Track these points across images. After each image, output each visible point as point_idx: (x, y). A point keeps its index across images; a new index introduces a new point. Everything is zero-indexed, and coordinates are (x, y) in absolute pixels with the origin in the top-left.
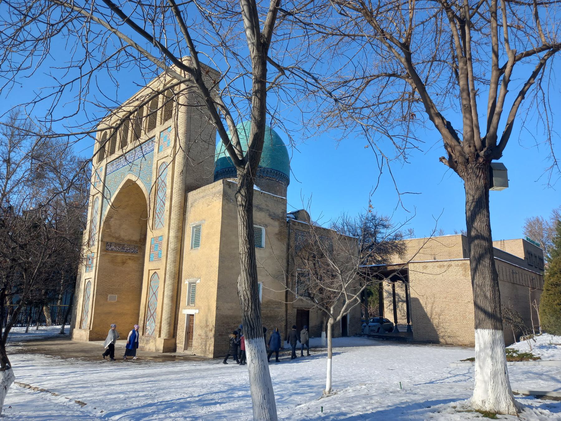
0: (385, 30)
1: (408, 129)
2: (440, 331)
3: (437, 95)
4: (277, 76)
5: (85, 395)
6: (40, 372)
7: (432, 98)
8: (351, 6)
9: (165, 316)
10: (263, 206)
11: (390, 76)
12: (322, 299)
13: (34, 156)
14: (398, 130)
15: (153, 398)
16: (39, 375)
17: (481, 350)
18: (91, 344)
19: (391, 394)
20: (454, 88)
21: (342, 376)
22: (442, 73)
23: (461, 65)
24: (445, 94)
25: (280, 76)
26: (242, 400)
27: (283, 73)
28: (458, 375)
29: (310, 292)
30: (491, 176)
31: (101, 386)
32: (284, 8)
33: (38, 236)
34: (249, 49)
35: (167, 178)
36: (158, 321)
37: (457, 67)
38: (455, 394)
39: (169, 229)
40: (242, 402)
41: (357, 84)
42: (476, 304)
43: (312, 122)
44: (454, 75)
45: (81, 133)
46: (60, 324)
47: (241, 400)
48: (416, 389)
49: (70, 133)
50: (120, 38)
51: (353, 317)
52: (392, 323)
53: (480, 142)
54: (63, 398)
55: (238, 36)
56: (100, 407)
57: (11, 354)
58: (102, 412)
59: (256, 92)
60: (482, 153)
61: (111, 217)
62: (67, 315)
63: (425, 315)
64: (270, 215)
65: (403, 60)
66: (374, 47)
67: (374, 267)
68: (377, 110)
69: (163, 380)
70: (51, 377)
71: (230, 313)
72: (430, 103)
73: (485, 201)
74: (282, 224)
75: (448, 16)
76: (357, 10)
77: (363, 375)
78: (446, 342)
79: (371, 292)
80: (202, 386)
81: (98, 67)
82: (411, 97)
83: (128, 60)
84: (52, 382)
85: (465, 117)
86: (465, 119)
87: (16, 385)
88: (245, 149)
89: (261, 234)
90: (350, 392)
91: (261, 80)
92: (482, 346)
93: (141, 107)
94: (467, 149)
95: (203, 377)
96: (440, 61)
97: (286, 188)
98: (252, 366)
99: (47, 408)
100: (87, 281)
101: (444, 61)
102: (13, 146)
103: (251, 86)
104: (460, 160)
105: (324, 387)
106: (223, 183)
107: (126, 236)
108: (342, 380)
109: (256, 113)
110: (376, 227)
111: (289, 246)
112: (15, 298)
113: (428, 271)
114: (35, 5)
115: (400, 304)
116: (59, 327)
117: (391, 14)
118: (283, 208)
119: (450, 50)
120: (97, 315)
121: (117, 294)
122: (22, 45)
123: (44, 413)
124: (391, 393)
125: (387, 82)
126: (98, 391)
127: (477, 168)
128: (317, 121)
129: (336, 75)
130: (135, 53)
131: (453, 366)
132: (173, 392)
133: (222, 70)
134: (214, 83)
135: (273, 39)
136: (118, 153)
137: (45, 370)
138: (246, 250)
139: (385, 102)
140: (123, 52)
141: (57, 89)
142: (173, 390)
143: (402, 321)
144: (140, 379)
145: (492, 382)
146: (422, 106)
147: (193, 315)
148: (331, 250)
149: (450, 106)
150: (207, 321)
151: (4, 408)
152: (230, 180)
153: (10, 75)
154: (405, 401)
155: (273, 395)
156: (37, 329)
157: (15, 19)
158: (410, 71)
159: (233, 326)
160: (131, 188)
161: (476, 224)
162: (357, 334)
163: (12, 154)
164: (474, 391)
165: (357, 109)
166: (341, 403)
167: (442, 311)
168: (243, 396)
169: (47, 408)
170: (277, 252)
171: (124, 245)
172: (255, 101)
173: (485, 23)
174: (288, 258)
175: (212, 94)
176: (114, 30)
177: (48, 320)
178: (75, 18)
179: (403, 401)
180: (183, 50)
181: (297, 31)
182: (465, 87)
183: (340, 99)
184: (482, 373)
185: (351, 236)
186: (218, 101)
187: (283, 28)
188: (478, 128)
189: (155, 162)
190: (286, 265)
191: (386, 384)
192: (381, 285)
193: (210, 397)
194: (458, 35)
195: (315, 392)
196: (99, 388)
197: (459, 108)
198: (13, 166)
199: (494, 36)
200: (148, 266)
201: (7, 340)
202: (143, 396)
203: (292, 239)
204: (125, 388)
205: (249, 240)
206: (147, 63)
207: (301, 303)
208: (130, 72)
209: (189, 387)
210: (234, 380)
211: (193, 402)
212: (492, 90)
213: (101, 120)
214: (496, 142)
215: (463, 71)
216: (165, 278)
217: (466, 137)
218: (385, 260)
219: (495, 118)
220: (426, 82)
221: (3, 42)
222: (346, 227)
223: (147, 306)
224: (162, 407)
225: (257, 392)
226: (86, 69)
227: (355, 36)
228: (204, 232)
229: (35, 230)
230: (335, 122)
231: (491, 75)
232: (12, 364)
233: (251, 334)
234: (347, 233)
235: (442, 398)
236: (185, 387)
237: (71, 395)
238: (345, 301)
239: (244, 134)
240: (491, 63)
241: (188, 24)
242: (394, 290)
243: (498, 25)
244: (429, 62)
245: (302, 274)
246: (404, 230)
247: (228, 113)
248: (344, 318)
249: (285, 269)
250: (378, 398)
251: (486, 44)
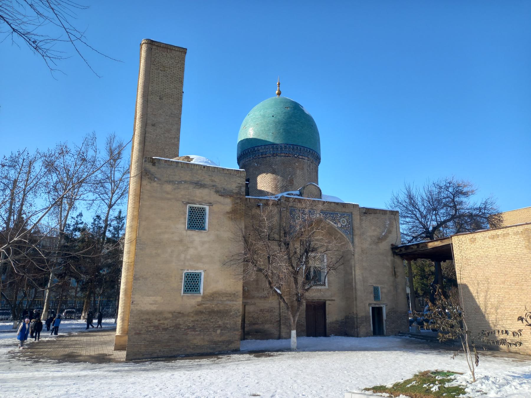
63: (478, 308)
64: (217, 192)
71: (154, 308)
74: (238, 201)
159: (157, 323)
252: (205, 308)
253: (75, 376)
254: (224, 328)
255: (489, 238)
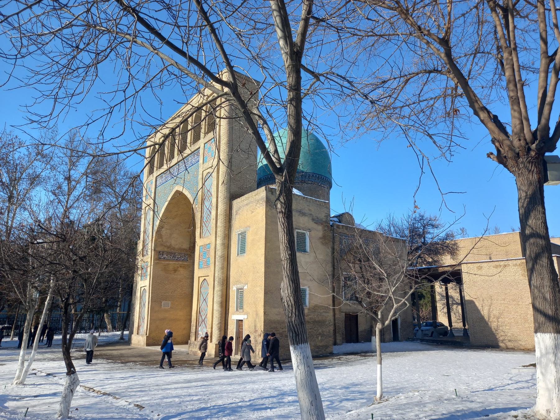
0: (422, 27)
1: (453, 125)
2: (500, 334)
3: (483, 88)
4: (311, 83)
5: (144, 398)
6: (102, 377)
7: (476, 92)
8: (385, 6)
9: (216, 321)
10: (306, 211)
11: (430, 72)
12: (371, 303)
13: (90, 172)
14: (442, 127)
15: (206, 402)
16: (102, 379)
17: (542, 356)
18: (148, 349)
19: (446, 402)
20: (500, 79)
21: (394, 383)
22: (487, 65)
23: (505, 55)
24: (492, 87)
25: (315, 82)
26: (292, 405)
27: (318, 79)
28: (520, 382)
29: (358, 296)
30: (546, 170)
31: (158, 390)
32: (316, 15)
33: (96, 248)
34: (284, 59)
35: (213, 187)
36: (209, 326)
37: (502, 56)
38: (516, 402)
39: (216, 237)
40: (292, 408)
41: (395, 84)
42: (534, 307)
43: (350, 125)
44: (500, 67)
45: (129, 151)
46: (119, 330)
47: (291, 405)
48: (473, 396)
49: (119, 152)
50: (162, 59)
51: (404, 321)
52: (447, 327)
53: (531, 135)
54: (123, 401)
55: (273, 46)
56: (157, 410)
57: (77, 359)
58: (159, 415)
59: (291, 100)
60: (534, 146)
61: (163, 227)
62: (125, 322)
63: (482, 318)
64: (313, 220)
65: (443, 55)
66: (411, 46)
67: (424, 269)
68: (418, 108)
69: (215, 385)
70: (112, 381)
72: (474, 98)
73: (539, 196)
74: (326, 228)
75: (490, 6)
76: (392, 9)
77: (416, 381)
78: (506, 346)
79: (422, 294)
80: (253, 391)
81: (143, 87)
82: (454, 92)
83: (170, 79)
84: (113, 386)
85: (512, 109)
86: (513, 112)
87: (82, 388)
88: (283, 156)
89: (305, 239)
90: (402, 398)
91: (296, 88)
92: (544, 351)
93: (185, 121)
94: (516, 143)
95: (254, 382)
96: (483, 52)
97: (329, 191)
98: (299, 372)
99: (109, 410)
100: (143, 289)
101: (489, 53)
102: (73, 164)
103: (286, 95)
104: (510, 155)
105: (375, 393)
106: (266, 190)
107: (177, 245)
108: (394, 387)
109: (292, 121)
110: (424, 227)
111: (333, 249)
112: (80, 306)
113: (483, 272)
114: (86, 35)
115: (455, 306)
116: (119, 333)
117: (428, 9)
118: (326, 212)
119: (494, 41)
120: (152, 321)
121: (170, 300)
122: (76, 72)
123: (107, 415)
124: (446, 400)
125: (428, 78)
126: (155, 394)
127: (529, 162)
128: (356, 124)
129: (373, 76)
130: (177, 72)
131: (514, 372)
132: (225, 396)
133: (261, 80)
134: (251, 94)
135: (307, 45)
136: (165, 167)
137: (106, 375)
138: (287, 257)
139: (426, 100)
140: (165, 72)
141: (107, 111)
142: (225, 394)
143: (458, 324)
144: (194, 384)
145: (557, 390)
146: (464, 101)
147: (242, 320)
148: (377, 252)
149: (496, 99)
150: (255, 327)
151: (71, 410)
152: (271, 187)
153: (66, 101)
154: (461, 408)
155: (321, 402)
156: (99, 335)
157: (69, 50)
158: (450, 66)
160: (179, 197)
161: (530, 221)
162: (409, 339)
163: (72, 172)
164: (537, 399)
165: (396, 108)
166: (392, 410)
167: (501, 314)
168: (293, 402)
169: (109, 410)
170: (321, 257)
171: (175, 253)
172: (291, 109)
173: (532, 9)
174: (334, 260)
175: (249, 105)
176: (156, 51)
177: (109, 327)
178: (120, 43)
179: (458, 409)
180: (220, 66)
181: (332, 35)
182: (512, 78)
183: (377, 101)
184: (544, 381)
185: (399, 237)
186: (255, 111)
187: (316, 35)
188: (528, 120)
189: (201, 172)
190: (331, 269)
191: (442, 391)
192: (433, 287)
193: (261, 402)
194: (501, 24)
195: (366, 398)
196: (156, 392)
197: (507, 100)
198: (73, 183)
199: (542, 22)
200: (197, 273)
201: (72, 346)
202: (197, 400)
203: (337, 243)
204: (179, 392)
205: (290, 247)
206: (188, 80)
207: (349, 307)
208: (173, 89)
209: (240, 392)
210: (284, 385)
211: (245, 407)
212: (542, 79)
213: (146, 138)
214: (548, 133)
215: (509, 61)
216: (214, 284)
217: (515, 130)
218: (436, 261)
219: (546, 108)
220: (469, 76)
221: (59, 71)
222: (392, 229)
223: (199, 312)
224: (215, 411)
225: (304, 398)
226: (130, 91)
227: (389, 35)
228: (249, 238)
229: (93, 243)
230: (375, 123)
231: (540, 64)
232: (77, 369)
233: (296, 340)
234: (394, 236)
235: (501, 406)
236: (237, 392)
237: (130, 398)
238: (393, 305)
239: (280, 142)
240: (540, 52)
241: (223, 40)
242: (447, 293)
243: (545, 9)
244: (471, 55)
245: (348, 278)
246: (455, 229)
247: (265, 122)
248: (395, 322)
249: (330, 273)
250: (431, 406)
251: (534, 30)
252: (310, 319)
253: (215, 380)
254: (322, 335)
255: (494, 267)
